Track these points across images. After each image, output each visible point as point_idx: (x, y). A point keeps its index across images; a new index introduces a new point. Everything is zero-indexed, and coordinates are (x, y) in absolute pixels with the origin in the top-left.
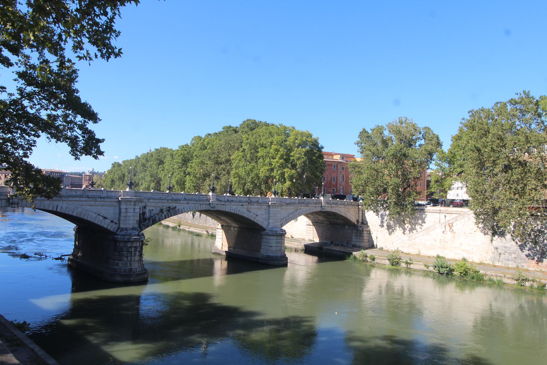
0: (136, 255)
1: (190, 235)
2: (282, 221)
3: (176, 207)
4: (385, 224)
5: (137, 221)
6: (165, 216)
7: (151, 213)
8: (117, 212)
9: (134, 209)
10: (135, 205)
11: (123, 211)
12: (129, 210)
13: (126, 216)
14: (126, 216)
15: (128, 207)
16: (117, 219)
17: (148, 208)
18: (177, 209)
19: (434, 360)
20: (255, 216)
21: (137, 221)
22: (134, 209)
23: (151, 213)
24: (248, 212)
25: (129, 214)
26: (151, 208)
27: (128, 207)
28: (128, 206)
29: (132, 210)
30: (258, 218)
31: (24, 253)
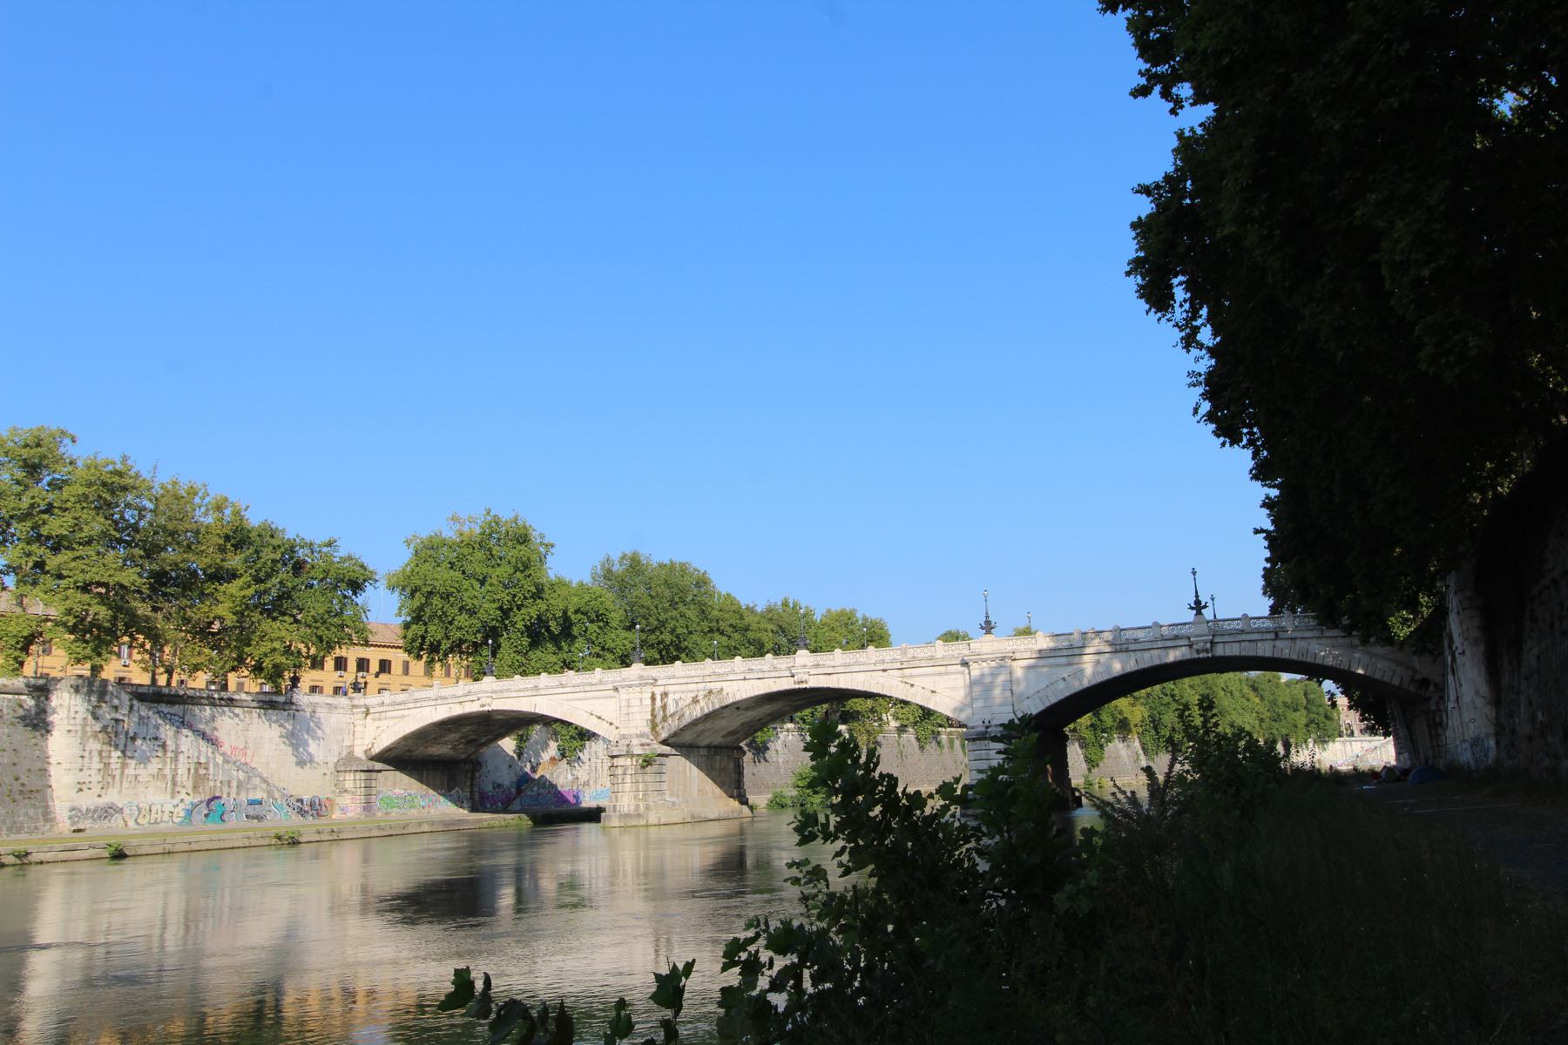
0: (625, 781)
1: (1031, 670)
2: (801, 722)
3: (722, 689)
4: (113, 743)
5: (647, 720)
6: (701, 708)
7: (677, 704)
10: (641, 692)
12: (633, 702)
13: (628, 714)
14: (628, 714)
15: (631, 696)
17: (671, 696)
18: (724, 693)
19: (955, 790)
20: (928, 694)
21: (647, 720)
23: (677, 704)
24: (904, 685)
25: (632, 710)
26: (677, 696)
27: (631, 696)
28: (557, 683)
30: (936, 698)
31: (690, 741)
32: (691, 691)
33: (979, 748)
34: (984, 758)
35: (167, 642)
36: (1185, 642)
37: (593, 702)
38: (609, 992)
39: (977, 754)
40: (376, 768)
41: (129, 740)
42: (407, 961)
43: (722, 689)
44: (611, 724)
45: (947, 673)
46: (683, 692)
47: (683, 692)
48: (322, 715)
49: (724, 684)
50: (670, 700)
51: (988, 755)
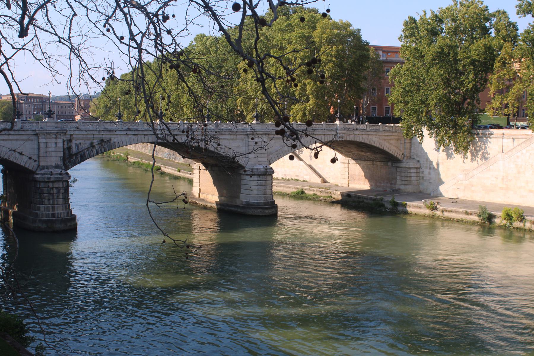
5: (60, 157)
8: (36, 147)
9: (56, 143)
11: (42, 145)
12: (50, 145)
13: (46, 152)
14: (46, 152)
16: (36, 156)
22: (56, 143)
25: (50, 149)
26: (78, 142)
27: (48, 140)
29: (53, 145)
32: (88, 139)
33: (261, 179)
34: (263, 184)
35: (285, 136)
36: (335, 133)
37: (14, 142)
38: (468, 313)
39: (260, 183)
40: (403, 186)
41: (246, 173)
42: (233, 348)
43: (110, 140)
44: (30, 158)
45: (236, 139)
46: (82, 140)
47: (82, 140)
48: (251, 162)
49: (112, 137)
50: (73, 144)
51: (266, 183)
